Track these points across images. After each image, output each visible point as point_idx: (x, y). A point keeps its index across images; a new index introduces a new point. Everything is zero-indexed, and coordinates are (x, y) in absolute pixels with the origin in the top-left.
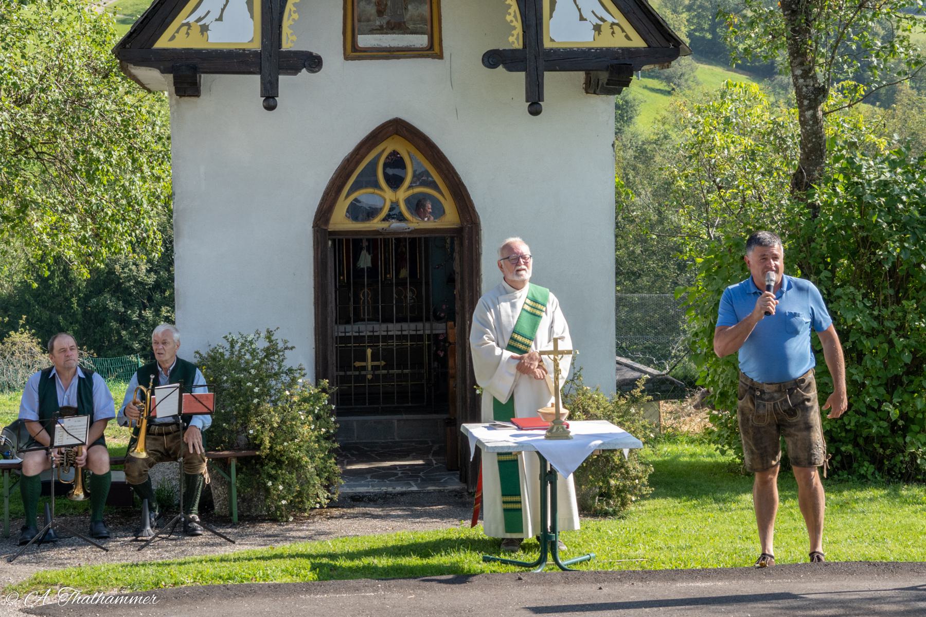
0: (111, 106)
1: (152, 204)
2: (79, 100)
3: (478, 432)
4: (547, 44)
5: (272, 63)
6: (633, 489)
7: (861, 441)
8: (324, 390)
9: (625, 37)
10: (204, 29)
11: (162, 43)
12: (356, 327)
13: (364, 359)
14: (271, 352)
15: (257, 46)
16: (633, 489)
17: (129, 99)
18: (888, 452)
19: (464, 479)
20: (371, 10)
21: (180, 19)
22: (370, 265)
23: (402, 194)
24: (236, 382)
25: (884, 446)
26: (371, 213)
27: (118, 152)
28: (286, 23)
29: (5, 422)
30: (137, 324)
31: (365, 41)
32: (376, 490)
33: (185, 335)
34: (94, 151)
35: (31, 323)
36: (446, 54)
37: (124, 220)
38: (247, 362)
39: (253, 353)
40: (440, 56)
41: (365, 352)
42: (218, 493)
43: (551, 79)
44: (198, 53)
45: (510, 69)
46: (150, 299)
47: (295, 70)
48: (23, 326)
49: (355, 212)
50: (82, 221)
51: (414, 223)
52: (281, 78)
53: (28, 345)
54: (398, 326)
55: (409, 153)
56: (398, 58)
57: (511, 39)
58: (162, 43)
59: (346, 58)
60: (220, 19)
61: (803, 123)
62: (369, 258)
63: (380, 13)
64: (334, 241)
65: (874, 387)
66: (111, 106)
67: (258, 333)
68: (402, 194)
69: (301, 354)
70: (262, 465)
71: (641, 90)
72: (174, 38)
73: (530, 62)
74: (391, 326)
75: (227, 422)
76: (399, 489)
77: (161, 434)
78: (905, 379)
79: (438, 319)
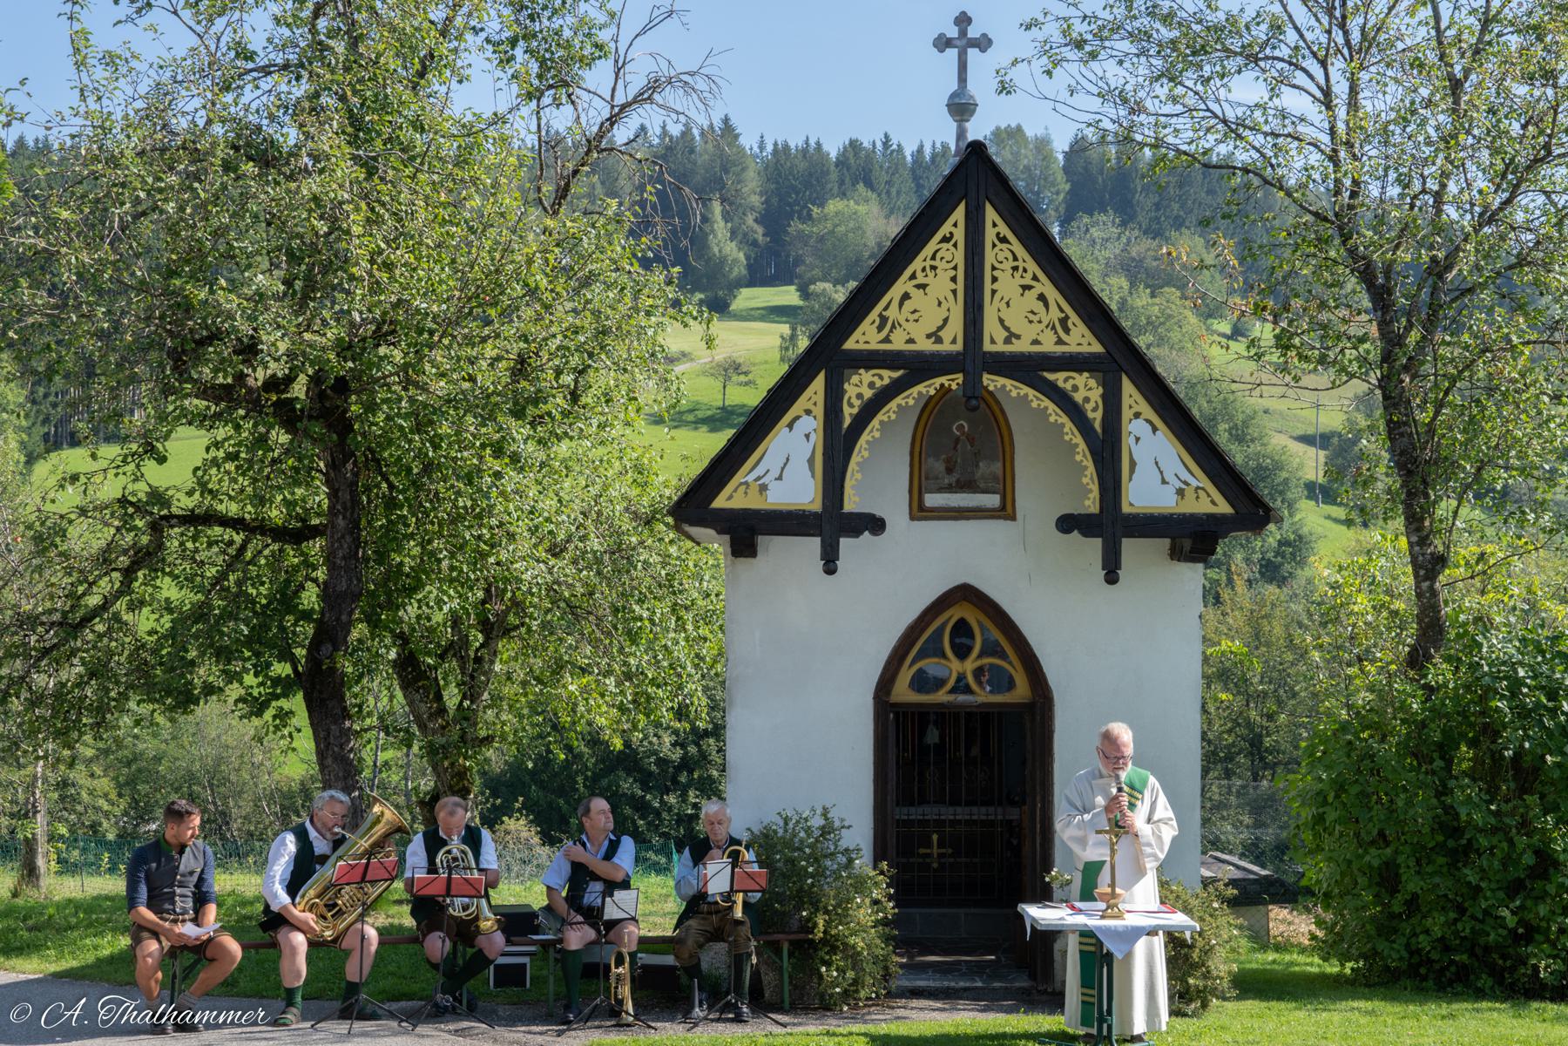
0: (655, 559)
1: (696, 666)
2: (621, 553)
3: (1039, 914)
4: (1126, 509)
5: (833, 525)
6: (1213, 992)
7: (1478, 951)
8: (882, 873)
9: (1211, 502)
10: (763, 488)
11: (720, 502)
12: (920, 810)
13: (929, 845)
14: (827, 830)
15: (817, 507)
16: (1213, 992)
17: (673, 550)
18: (1508, 963)
19: (1033, 977)
20: (939, 466)
22: (937, 740)
23: (969, 665)
24: (791, 865)
25: (1504, 957)
26: (940, 683)
27: (662, 609)
28: (849, 483)
30: (658, 813)
31: (932, 500)
32: (937, 984)
33: (742, 808)
34: (636, 608)
35: (528, 808)
37: (666, 684)
38: (802, 841)
39: (808, 830)
40: (1013, 518)
41: (930, 837)
42: (768, 978)
43: (1129, 546)
45: (1085, 535)
46: (675, 781)
47: (856, 532)
48: (519, 810)
49: (921, 682)
50: (619, 684)
51: (983, 696)
53: (524, 835)
54: (967, 809)
55: (979, 622)
56: (968, 518)
57: (1087, 503)
58: (720, 502)
59: (912, 518)
60: (780, 478)
61: (1419, 595)
62: (936, 733)
63: (949, 471)
64: (897, 715)
65: (1493, 891)
66: (655, 559)
67: (813, 810)
68: (969, 665)
69: (858, 833)
70: (816, 950)
71: (1322, 521)
72: (729, 499)
73: (1109, 528)
74: (959, 810)
75: (780, 903)
76: (962, 984)
77: (710, 913)
78: (1528, 883)
79: (1013, 803)
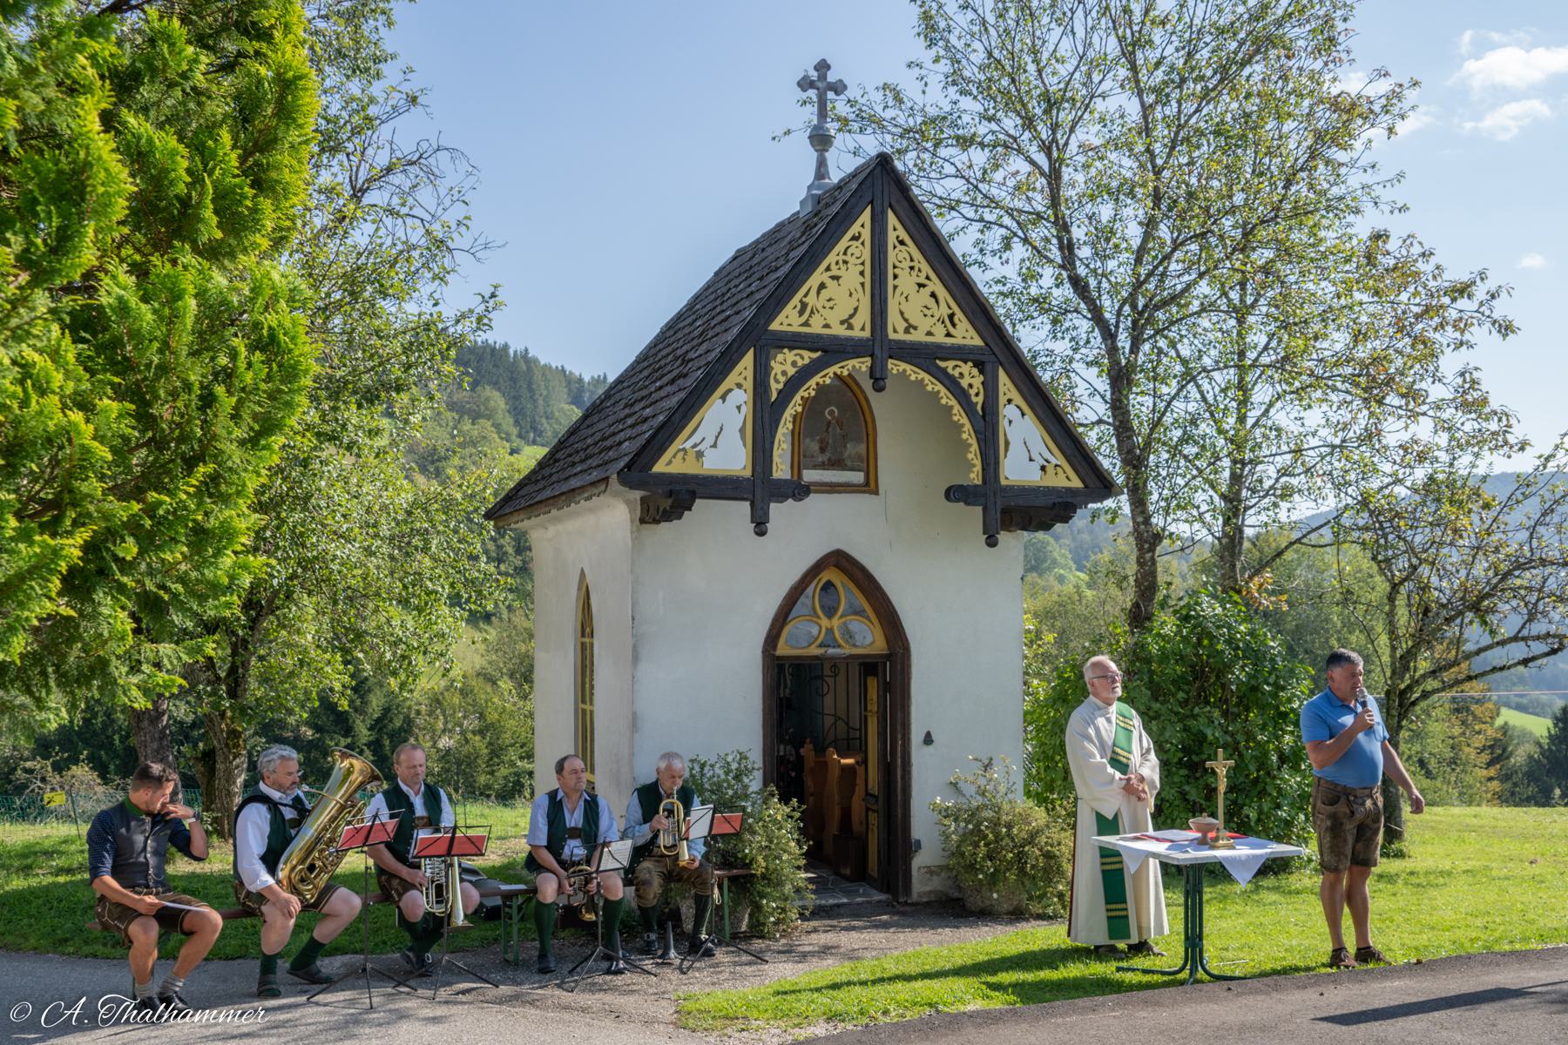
4: (1003, 482)
10: (700, 455)
11: (660, 467)
21: (677, 444)
29: (1422, 882)
36: (881, 491)
40: (876, 492)
44: (694, 478)
52: (772, 505)
57: (972, 476)
58: (660, 467)
60: (715, 446)
63: (822, 450)
76: (831, 902)
